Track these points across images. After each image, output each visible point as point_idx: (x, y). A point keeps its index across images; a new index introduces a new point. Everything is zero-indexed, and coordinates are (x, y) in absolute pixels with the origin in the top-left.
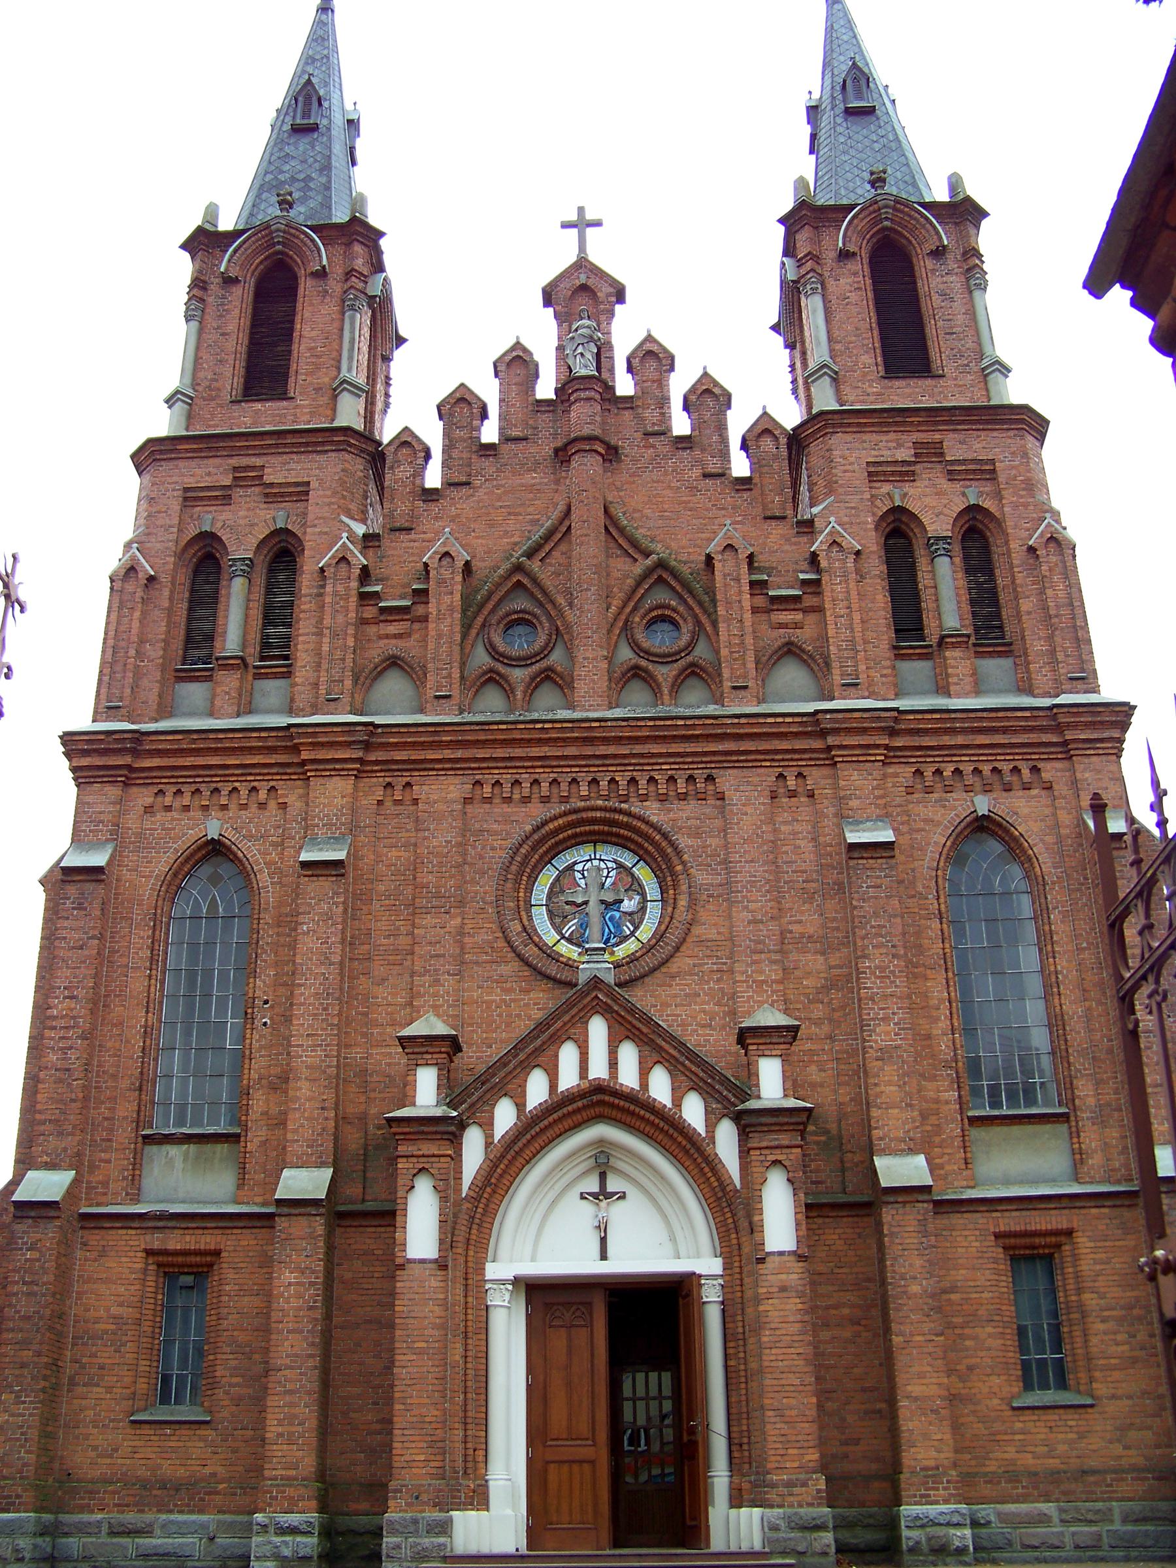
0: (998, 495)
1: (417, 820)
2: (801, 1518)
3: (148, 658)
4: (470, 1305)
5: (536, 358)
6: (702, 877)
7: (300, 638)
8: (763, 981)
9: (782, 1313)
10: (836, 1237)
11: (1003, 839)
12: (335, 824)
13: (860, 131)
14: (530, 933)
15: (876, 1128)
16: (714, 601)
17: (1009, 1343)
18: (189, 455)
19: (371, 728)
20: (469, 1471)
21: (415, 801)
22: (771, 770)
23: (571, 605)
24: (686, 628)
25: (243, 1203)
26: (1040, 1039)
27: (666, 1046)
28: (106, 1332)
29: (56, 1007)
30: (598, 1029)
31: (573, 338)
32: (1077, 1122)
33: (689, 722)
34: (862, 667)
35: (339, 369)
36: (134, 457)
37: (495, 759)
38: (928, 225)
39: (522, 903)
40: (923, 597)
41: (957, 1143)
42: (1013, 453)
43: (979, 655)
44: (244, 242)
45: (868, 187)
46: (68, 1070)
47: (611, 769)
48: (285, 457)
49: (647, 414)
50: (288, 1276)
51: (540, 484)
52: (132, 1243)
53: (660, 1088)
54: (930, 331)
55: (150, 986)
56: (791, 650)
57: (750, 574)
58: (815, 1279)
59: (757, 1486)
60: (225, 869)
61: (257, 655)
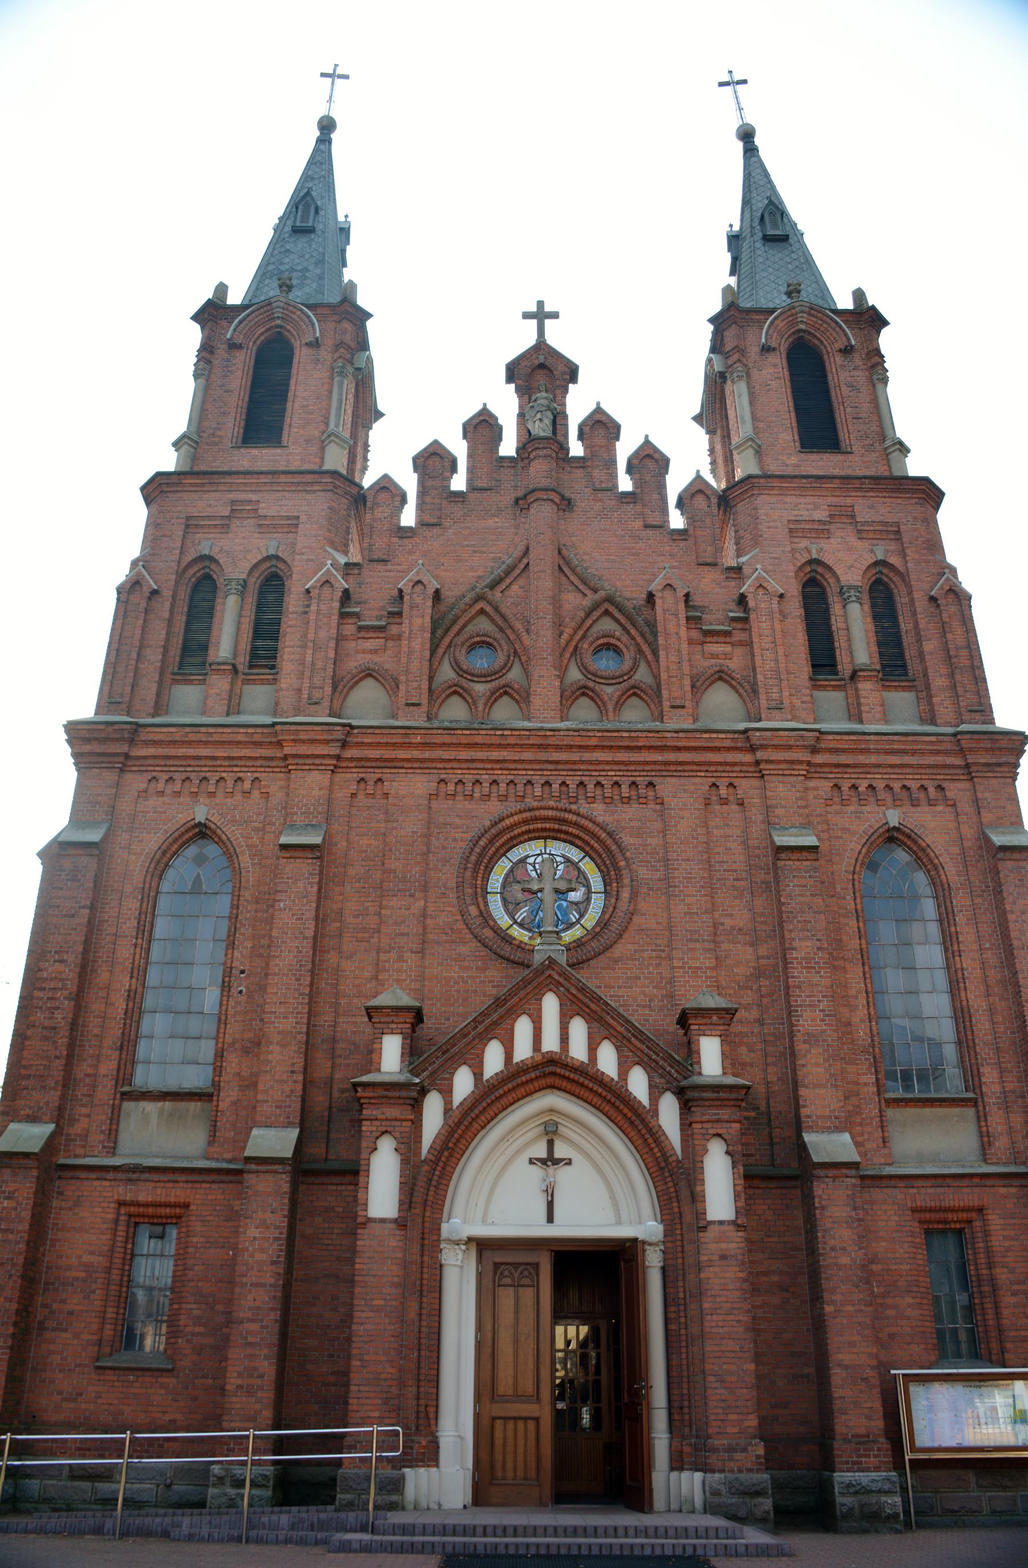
0: (903, 553)
1: (387, 813)
2: (742, 1484)
3: (149, 661)
4: (425, 1265)
5: (500, 422)
6: (643, 872)
7: (286, 650)
8: (699, 968)
9: (722, 1281)
10: (766, 1207)
11: (911, 849)
12: (313, 813)
13: (776, 254)
14: (486, 917)
15: (804, 1106)
16: (655, 634)
17: (926, 1313)
18: (192, 489)
19: (348, 728)
20: (421, 1428)
21: (386, 795)
22: (705, 779)
23: (528, 631)
24: (628, 656)
25: (213, 1159)
26: (946, 1031)
27: (615, 1024)
28: (76, 1279)
29: (46, 970)
30: (550, 1005)
31: (532, 407)
32: (984, 1108)
33: (633, 734)
34: (786, 694)
35: (327, 424)
36: (143, 489)
37: (459, 761)
38: (838, 329)
39: (479, 890)
40: (836, 637)
41: (876, 1121)
42: (915, 518)
43: (886, 688)
44: (248, 315)
45: (784, 297)
46: (54, 1028)
47: (562, 773)
48: (278, 494)
49: (596, 473)
50: (253, 1232)
51: (502, 527)
52: (105, 1194)
53: (607, 1060)
54: (839, 416)
55: (135, 954)
56: (722, 676)
57: (687, 611)
58: (751, 1246)
59: (696, 1450)
60: (212, 850)
61: (247, 664)
